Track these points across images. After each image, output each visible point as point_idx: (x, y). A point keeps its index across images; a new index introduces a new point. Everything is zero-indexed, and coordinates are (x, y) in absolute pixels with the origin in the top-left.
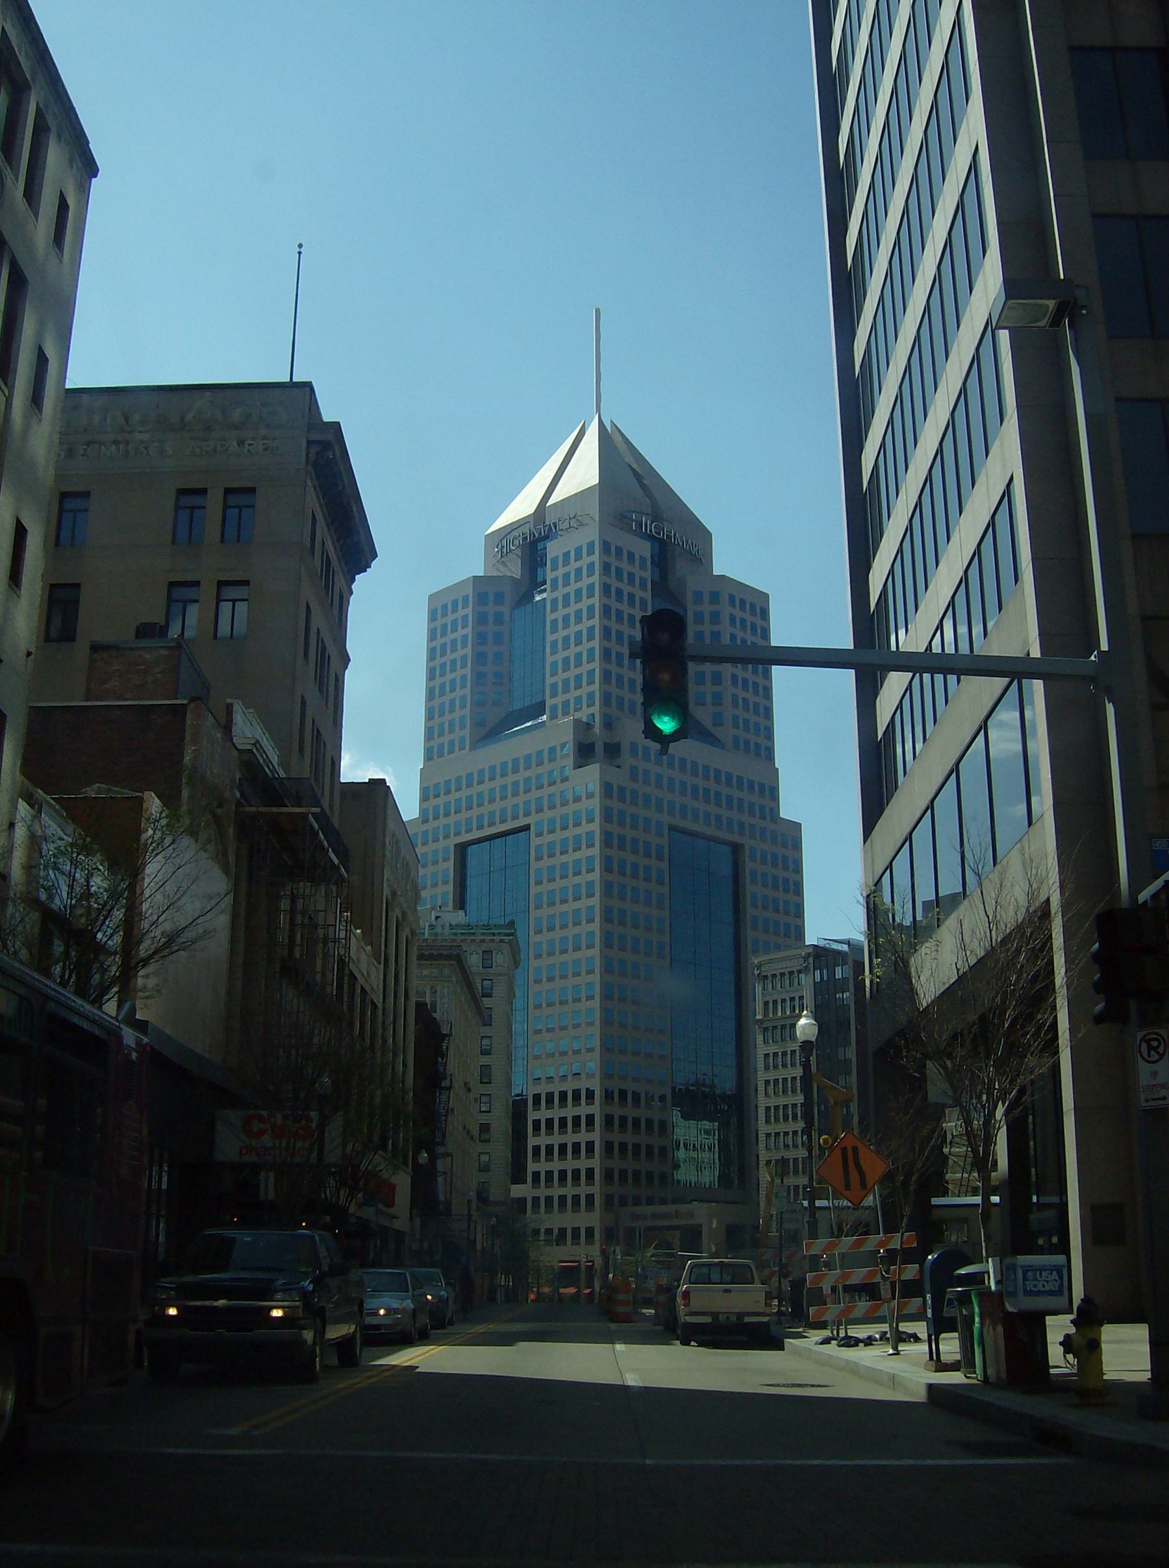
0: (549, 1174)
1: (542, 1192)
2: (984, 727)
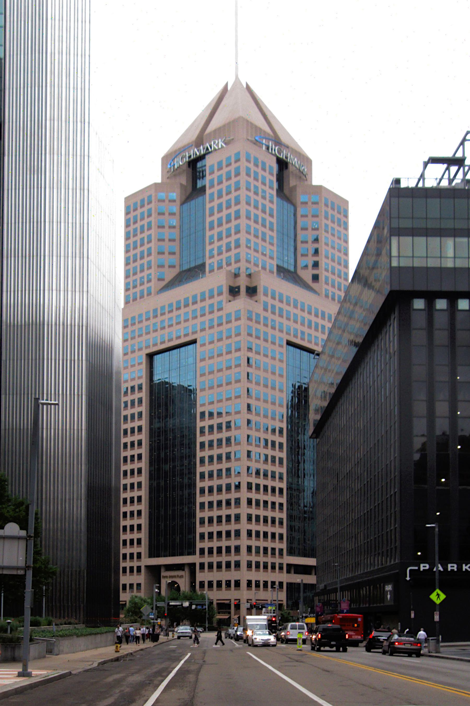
0: (211, 427)
1: (206, 560)
2: (462, 143)
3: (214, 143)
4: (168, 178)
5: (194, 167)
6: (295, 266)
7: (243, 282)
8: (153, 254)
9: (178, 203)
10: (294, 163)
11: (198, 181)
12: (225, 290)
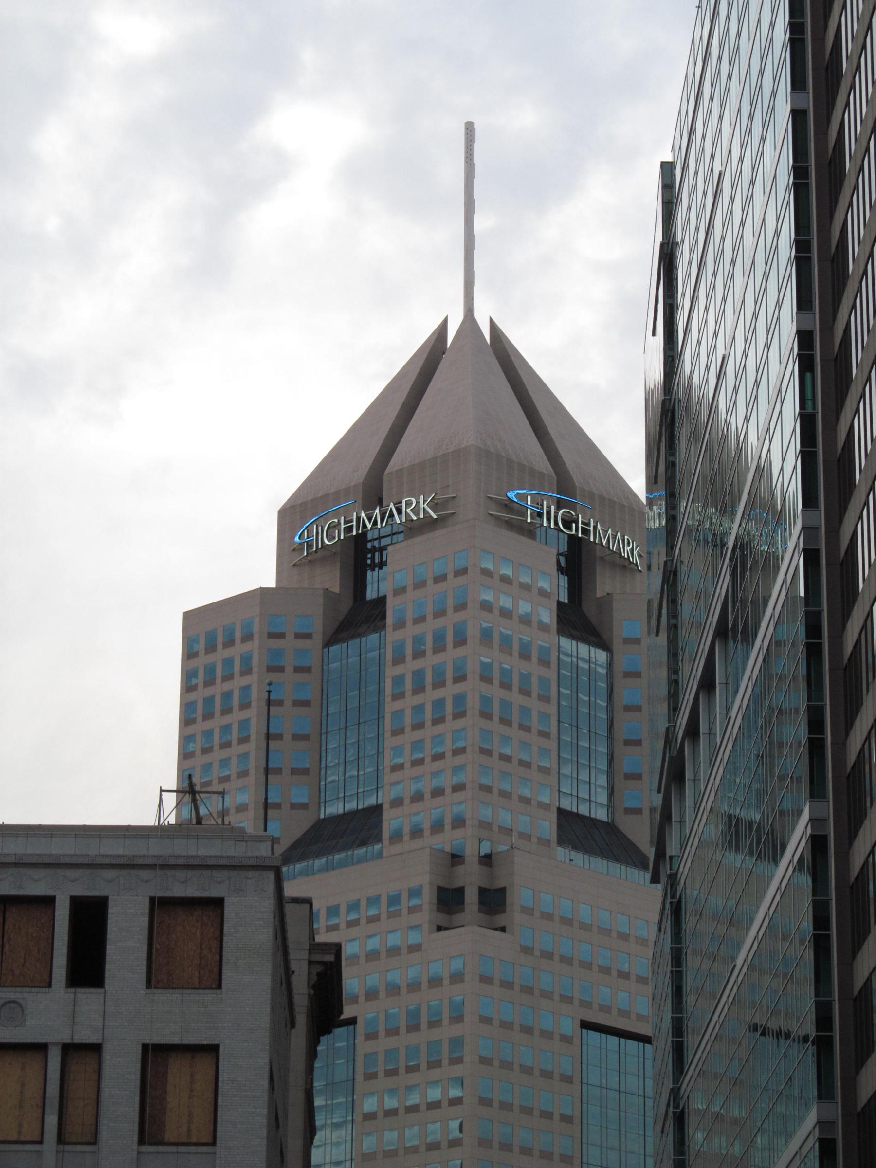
3: (408, 504)
4: (294, 565)
5: (361, 555)
6: (611, 806)
7: (470, 878)
8: (255, 670)
9: (318, 639)
10: (604, 542)
11: (369, 573)
12: (428, 897)
